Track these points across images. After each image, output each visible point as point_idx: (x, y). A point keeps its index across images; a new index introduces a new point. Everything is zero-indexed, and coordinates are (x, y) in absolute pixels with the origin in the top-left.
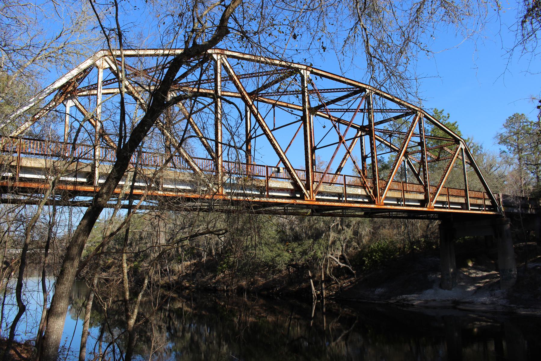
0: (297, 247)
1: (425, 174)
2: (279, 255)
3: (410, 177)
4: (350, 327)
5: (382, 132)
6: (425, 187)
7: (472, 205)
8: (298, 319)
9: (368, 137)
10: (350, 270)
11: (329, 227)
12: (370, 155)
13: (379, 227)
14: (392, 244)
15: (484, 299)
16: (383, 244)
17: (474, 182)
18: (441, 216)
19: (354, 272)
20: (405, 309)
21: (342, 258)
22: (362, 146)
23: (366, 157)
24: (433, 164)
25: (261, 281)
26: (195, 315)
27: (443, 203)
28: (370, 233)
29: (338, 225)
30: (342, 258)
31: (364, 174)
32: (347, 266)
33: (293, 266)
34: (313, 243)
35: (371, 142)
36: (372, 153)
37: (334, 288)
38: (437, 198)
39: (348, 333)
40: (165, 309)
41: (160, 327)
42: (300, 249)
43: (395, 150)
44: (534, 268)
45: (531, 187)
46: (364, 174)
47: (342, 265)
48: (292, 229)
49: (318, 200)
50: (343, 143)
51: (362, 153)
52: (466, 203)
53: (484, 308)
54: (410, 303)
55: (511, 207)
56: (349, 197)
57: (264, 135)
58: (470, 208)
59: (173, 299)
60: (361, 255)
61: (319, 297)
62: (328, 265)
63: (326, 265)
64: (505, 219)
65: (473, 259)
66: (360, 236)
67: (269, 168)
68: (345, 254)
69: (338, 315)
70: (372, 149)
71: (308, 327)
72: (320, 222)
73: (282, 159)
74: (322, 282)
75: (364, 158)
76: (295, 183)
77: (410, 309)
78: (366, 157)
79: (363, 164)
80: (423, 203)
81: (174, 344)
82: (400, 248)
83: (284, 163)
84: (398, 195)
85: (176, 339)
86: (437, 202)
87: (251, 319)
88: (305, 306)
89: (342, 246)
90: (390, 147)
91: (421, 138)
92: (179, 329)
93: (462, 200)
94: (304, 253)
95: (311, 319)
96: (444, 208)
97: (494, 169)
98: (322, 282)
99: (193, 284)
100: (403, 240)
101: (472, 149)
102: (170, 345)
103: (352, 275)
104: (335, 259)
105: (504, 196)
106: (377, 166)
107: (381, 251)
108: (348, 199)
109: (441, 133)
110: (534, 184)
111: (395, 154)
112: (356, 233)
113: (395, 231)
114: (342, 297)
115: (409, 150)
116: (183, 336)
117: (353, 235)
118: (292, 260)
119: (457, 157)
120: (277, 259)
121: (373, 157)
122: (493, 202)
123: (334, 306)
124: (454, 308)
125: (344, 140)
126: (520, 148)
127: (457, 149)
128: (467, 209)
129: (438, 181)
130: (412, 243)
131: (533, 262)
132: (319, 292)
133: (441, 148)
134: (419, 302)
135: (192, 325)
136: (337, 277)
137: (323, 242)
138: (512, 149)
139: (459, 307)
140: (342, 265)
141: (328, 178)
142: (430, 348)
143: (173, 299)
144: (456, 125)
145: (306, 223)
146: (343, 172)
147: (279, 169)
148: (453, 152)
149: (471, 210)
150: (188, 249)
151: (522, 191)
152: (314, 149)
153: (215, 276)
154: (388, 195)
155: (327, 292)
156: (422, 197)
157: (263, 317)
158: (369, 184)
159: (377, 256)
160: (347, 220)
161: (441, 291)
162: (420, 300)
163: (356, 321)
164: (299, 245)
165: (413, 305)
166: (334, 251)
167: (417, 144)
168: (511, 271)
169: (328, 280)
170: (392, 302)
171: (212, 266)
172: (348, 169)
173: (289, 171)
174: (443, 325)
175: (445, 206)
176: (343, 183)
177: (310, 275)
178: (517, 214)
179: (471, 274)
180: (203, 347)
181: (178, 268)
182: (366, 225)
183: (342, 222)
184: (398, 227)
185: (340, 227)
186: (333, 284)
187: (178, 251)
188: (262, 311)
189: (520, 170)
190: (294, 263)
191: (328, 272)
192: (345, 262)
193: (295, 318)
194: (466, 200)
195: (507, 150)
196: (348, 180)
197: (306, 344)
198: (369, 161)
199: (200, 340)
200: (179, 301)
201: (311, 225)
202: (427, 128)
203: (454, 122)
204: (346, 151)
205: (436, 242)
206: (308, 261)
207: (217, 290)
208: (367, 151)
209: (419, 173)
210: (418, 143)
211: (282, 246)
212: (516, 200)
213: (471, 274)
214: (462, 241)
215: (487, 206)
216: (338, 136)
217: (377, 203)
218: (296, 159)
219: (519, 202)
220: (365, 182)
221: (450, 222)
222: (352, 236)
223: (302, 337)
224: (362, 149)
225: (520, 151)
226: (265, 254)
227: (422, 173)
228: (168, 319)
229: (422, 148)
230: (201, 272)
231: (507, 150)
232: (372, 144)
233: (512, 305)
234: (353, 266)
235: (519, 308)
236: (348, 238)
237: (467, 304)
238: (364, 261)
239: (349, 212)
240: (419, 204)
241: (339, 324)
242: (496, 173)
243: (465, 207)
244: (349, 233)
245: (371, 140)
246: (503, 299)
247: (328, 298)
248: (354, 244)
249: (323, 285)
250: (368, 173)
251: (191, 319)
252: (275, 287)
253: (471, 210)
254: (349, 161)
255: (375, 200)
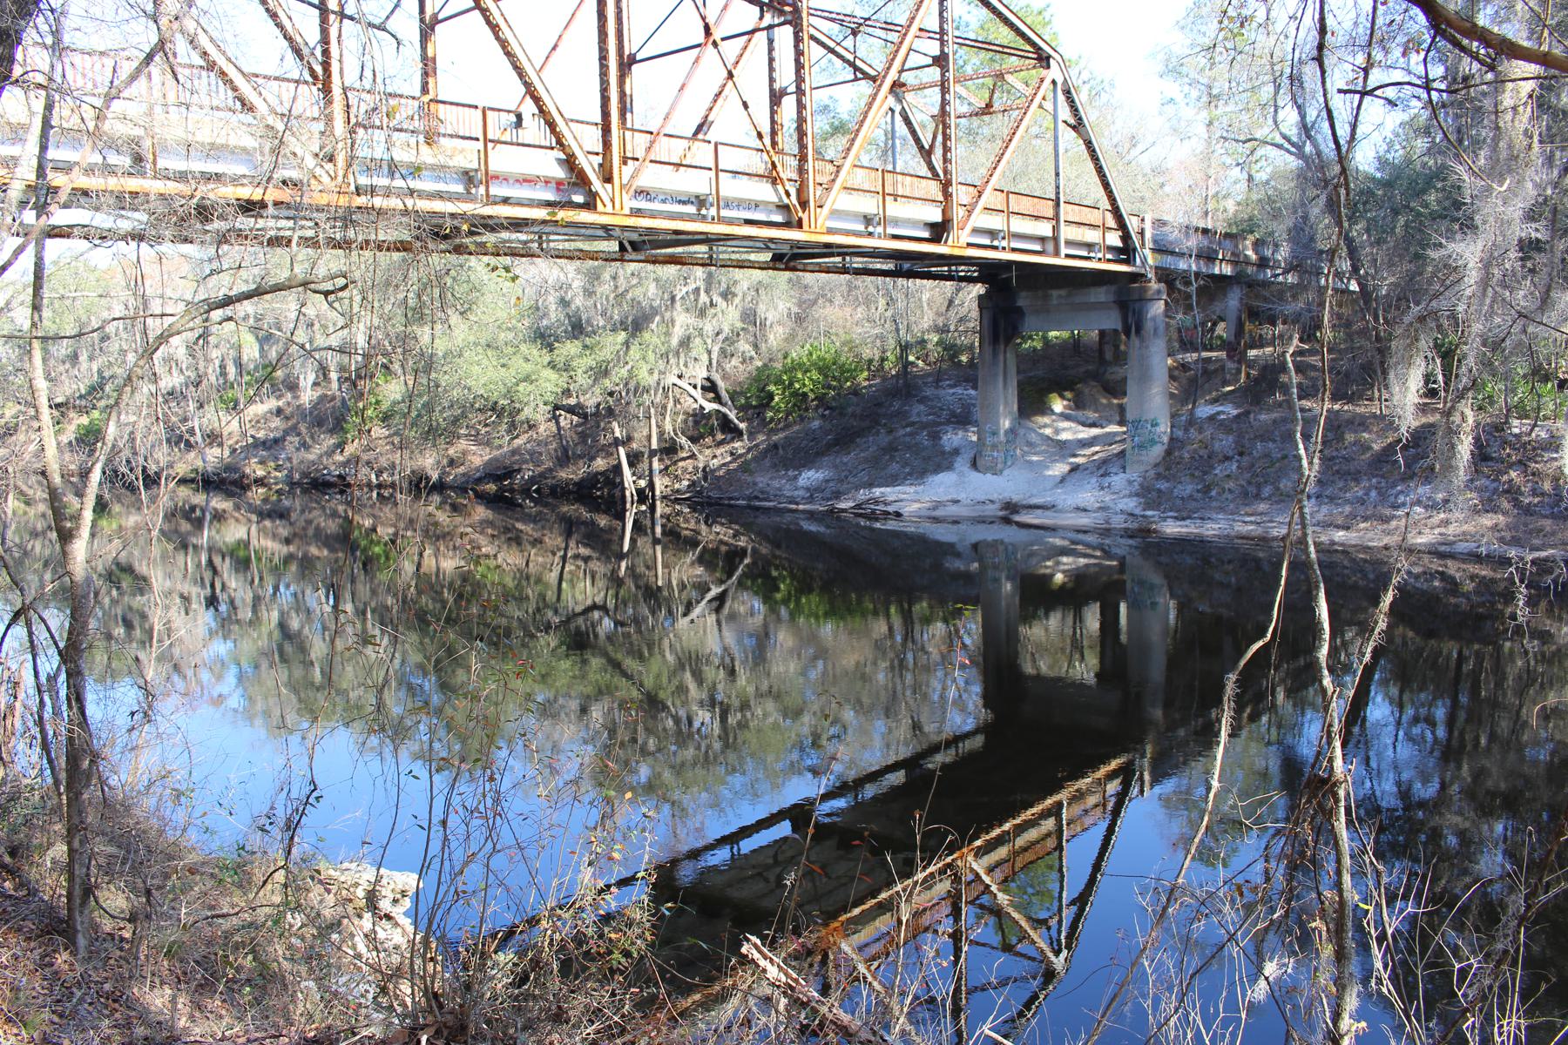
0: (581, 356)
1: (946, 150)
2: (527, 379)
3: (909, 159)
4: (730, 576)
5: (833, 20)
6: (946, 185)
7: (1069, 243)
8: (586, 559)
9: (788, 31)
10: (730, 421)
11: (673, 299)
12: (792, 88)
13: (815, 302)
14: (850, 350)
15: (1087, 495)
16: (826, 349)
17: (1081, 182)
18: (991, 273)
19: (742, 426)
20: (878, 525)
21: (710, 388)
22: (771, 60)
23: (784, 92)
24: (976, 121)
25: (478, 457)
26: (288, 559)
27: (992, 234)
28: (789, 315)
29: (697, 290)
30: (710, 388)
31: (774, 144)
32: (724, 410)
33: (571, 410)
34: (627, 344)
35: (796, 46)
36: (800, 79)
37: (685, 470)
38: (981, 220)
39: (724, 593)
40: (195, 547)
41: (186, 599)
42: (589, 361)
43: (866, 76)
44: (1212, 418)
45: (1231, 206)
46: (774, 144)
47: (710, 407)
48: (564, 303)
49: (637, 213)
50: (715, 44)
51: (772, 80)
52: (1055, 239)
53: (1084, 521)
54: (890, 509)
55: (1172, 253)
56: (727, 206)
57: (477, 12)
58: (1064, 251)
59: (219, 517)
60: (761, 380)
61: (642, 496)
62: (670, 405)
63: (664, 407)
64: (1154, 285)
65: (1068, 394)
66: (763, 325)
67: (489, 113)
68: (717, 378)
69: (697, 544)
70: (799, 67)
71: (615, 581)
72: (646, 281)
73: (528, 86)
74: (652, 453)
75: (776, 97)
76: (570, 162)
77: (891, 525)
78: (784, 92)
79: (773, 113)
80: (939, 231)
81: (230, 644)
82: (870, 361)
83: (537, 100)
84: (869, 205)
85: (236, 628)
86: (976, 231)
87: (449, 564)
88: (603, 521)
89: (709, 352)
90: (852, 65)
91: (943, 43)
92: (243, 600)
93: (1045, 229)
94: (602, 372)
95: (621, 556)
96: (996, 248)
97: (1140, 148)
98: (652, 453)
99: (278, 468)
100: (882, 338)
101: (1087, 87)
102: (221, 648)
103: (738, 434)
104: (690, 389)
105: (1159, 223)
106: (817, 125)
107: (820, 370)
108: (724, 213)
109: (1004, 35)
110: (1239, 198)
111: (865, 88)
112: (750, 317)
113: (861, 312)
114: (708, 499)
115: (905, 77)
116: (255, 622)
117: (743, 321)
118: (567, 392)
119: (1041, 107)
120: (521, 388)
121: (800, 92)
122: (1126, 237)
123: (687, 521)
124: (1007, 521)
125: (717, 35)
126: (1215, 92)
127: (1042, 80)
128: (1057, 253)
129: (984, 171)
130: (905, 348)
131: (1215, 401)
132: (643, 483)
133: (1000, 76)
134: (916, 506)
135: (282, 589)
136: (694, 440)
137: (655, 339)
138: (1195, 94)
139: (1017, 518)
140: (710, 407)
141: (669, 149)
142: (939, 628)
143: (219, 517)
144: (1047, 15)
145: (605, 288)
146: (713, 135)
147: (519, 117)
148: (1029, 91)
149: (1067, 256)
150: (256, 369)
151: (1206, 213)
152: (627, 63)
153: (341, 446)
154: (839, 206)
155: (666, 481)
156: (936, 216)
157: (487, 556)
158: (788, 170)
159: (807, 383)
160: (724, 276)
161: (974, 476)
162: (918, 501)
163: (747, 561)
164: (585, 347)
165: (898, 515)
166: (686, 365)
167: (930, 61)
168: (1155, 425)
169: (669, 449)
170: (842, 505)
171: (331, 419)
172: (731, 125)
173: (552, 125)
174: (976, 565)
175: (996, 243)
176: (712, 165)
177: (618, 434)
178: (1185, 277)
179: (1057, 431)
180: (318, 648)
181: (231, 426)
182: (777, 293)
183: (709, 280)
184: (868, 302)
185: (704, 298)
186: (684, 459)
187: (224, 374)
188: (482, 540)
189: (1207, 157)
190: (572, 401)
191: (668, 427)
192: (718, 399)
193: (576, 557)
194: (1056, 229)
195: (1179, 97)
196: (729, 159)
197: (607, 624)
198: (789, 103)
199: (306, 631)
200: (237, 520)
201: (620, 290)
202: (966, 18)
203: (1042, 6)
204: (725, 74)
205: (971, 347)
206: (611, 394)
207: (349, 485)
208: (786, 77)
209: (932, 146)
210: (934, 58)
211: (535, 352)
212: (1187, 234)
213: (1057, 431)
214: (1039, 345)
215: (1111, 249)
216: (702, 24)
217: (805, 226)
218: (574, 89)
219: (1193, 242)
220: (774, 165)
221: (1010, 289)
222: (739, 325)
223: (594, 607)
224: (771, 69)
225: (1213, 99)
226: (481, 376)
227: (938, 151)
228: (208, 575)
229: (943, 75)
230: (299, 434)
231: (1179, 97)
232: (799, 53)
233: (1149, 513)
234: (740, 409)
235: (1164, 519)
236: (726, 330)
237: (1039, 512)
238: (771, 396)
239: (724, 253)
240: (926, 235)
241: (700, 570)
242: (1144, 159)
243: (1050, 247)
244: (728, 316)
245: (798, 40)
246: (1130, 496)
247: (672, 499)
248: (744, 346)
249: (656, 465)
250: (788, 141)
251: (277, 572)
252: (519, 471)
253: (1067, 256)
254: (731, 101)
255: (800, 220)
